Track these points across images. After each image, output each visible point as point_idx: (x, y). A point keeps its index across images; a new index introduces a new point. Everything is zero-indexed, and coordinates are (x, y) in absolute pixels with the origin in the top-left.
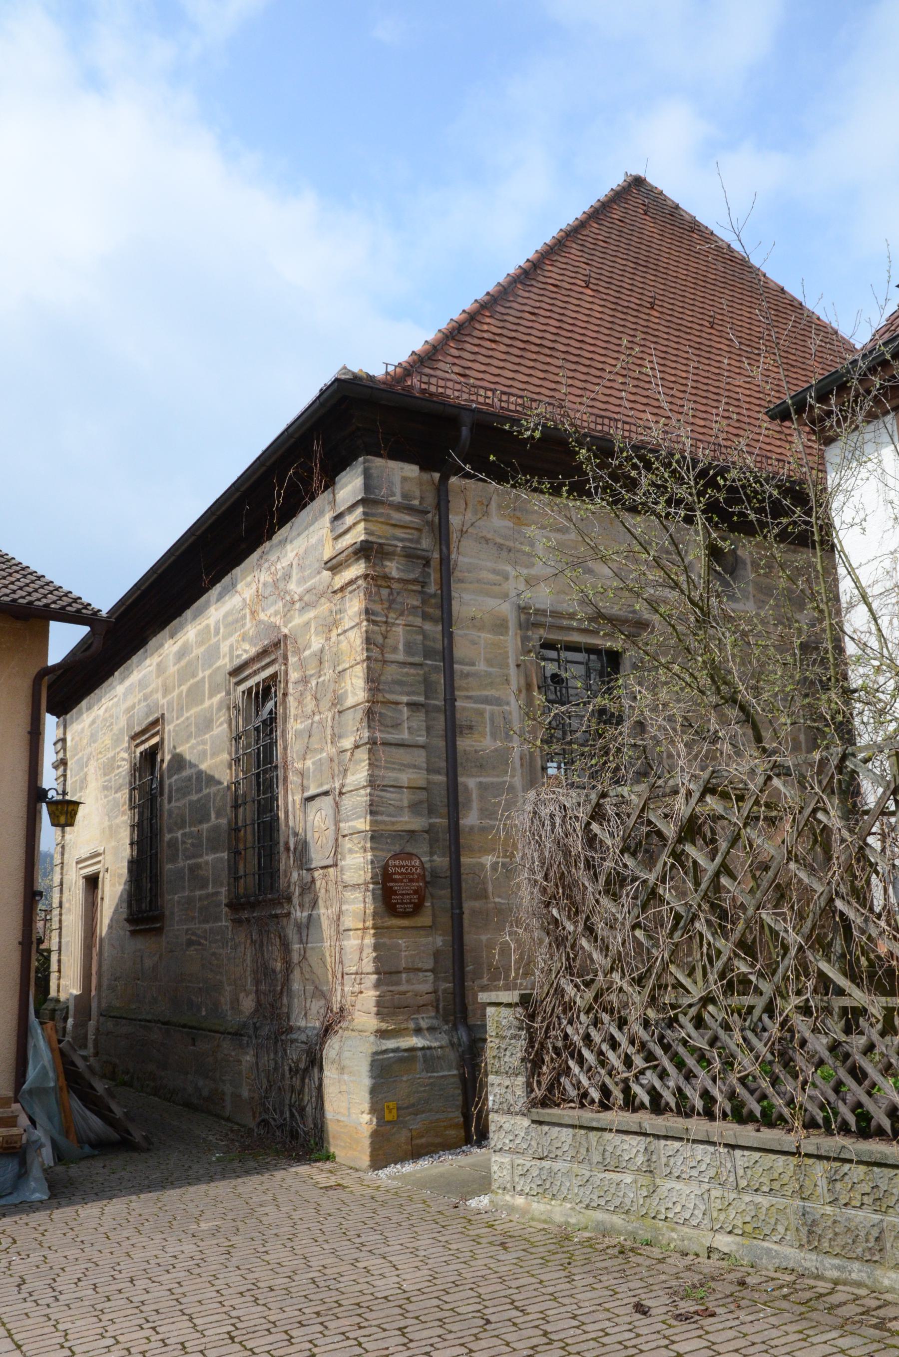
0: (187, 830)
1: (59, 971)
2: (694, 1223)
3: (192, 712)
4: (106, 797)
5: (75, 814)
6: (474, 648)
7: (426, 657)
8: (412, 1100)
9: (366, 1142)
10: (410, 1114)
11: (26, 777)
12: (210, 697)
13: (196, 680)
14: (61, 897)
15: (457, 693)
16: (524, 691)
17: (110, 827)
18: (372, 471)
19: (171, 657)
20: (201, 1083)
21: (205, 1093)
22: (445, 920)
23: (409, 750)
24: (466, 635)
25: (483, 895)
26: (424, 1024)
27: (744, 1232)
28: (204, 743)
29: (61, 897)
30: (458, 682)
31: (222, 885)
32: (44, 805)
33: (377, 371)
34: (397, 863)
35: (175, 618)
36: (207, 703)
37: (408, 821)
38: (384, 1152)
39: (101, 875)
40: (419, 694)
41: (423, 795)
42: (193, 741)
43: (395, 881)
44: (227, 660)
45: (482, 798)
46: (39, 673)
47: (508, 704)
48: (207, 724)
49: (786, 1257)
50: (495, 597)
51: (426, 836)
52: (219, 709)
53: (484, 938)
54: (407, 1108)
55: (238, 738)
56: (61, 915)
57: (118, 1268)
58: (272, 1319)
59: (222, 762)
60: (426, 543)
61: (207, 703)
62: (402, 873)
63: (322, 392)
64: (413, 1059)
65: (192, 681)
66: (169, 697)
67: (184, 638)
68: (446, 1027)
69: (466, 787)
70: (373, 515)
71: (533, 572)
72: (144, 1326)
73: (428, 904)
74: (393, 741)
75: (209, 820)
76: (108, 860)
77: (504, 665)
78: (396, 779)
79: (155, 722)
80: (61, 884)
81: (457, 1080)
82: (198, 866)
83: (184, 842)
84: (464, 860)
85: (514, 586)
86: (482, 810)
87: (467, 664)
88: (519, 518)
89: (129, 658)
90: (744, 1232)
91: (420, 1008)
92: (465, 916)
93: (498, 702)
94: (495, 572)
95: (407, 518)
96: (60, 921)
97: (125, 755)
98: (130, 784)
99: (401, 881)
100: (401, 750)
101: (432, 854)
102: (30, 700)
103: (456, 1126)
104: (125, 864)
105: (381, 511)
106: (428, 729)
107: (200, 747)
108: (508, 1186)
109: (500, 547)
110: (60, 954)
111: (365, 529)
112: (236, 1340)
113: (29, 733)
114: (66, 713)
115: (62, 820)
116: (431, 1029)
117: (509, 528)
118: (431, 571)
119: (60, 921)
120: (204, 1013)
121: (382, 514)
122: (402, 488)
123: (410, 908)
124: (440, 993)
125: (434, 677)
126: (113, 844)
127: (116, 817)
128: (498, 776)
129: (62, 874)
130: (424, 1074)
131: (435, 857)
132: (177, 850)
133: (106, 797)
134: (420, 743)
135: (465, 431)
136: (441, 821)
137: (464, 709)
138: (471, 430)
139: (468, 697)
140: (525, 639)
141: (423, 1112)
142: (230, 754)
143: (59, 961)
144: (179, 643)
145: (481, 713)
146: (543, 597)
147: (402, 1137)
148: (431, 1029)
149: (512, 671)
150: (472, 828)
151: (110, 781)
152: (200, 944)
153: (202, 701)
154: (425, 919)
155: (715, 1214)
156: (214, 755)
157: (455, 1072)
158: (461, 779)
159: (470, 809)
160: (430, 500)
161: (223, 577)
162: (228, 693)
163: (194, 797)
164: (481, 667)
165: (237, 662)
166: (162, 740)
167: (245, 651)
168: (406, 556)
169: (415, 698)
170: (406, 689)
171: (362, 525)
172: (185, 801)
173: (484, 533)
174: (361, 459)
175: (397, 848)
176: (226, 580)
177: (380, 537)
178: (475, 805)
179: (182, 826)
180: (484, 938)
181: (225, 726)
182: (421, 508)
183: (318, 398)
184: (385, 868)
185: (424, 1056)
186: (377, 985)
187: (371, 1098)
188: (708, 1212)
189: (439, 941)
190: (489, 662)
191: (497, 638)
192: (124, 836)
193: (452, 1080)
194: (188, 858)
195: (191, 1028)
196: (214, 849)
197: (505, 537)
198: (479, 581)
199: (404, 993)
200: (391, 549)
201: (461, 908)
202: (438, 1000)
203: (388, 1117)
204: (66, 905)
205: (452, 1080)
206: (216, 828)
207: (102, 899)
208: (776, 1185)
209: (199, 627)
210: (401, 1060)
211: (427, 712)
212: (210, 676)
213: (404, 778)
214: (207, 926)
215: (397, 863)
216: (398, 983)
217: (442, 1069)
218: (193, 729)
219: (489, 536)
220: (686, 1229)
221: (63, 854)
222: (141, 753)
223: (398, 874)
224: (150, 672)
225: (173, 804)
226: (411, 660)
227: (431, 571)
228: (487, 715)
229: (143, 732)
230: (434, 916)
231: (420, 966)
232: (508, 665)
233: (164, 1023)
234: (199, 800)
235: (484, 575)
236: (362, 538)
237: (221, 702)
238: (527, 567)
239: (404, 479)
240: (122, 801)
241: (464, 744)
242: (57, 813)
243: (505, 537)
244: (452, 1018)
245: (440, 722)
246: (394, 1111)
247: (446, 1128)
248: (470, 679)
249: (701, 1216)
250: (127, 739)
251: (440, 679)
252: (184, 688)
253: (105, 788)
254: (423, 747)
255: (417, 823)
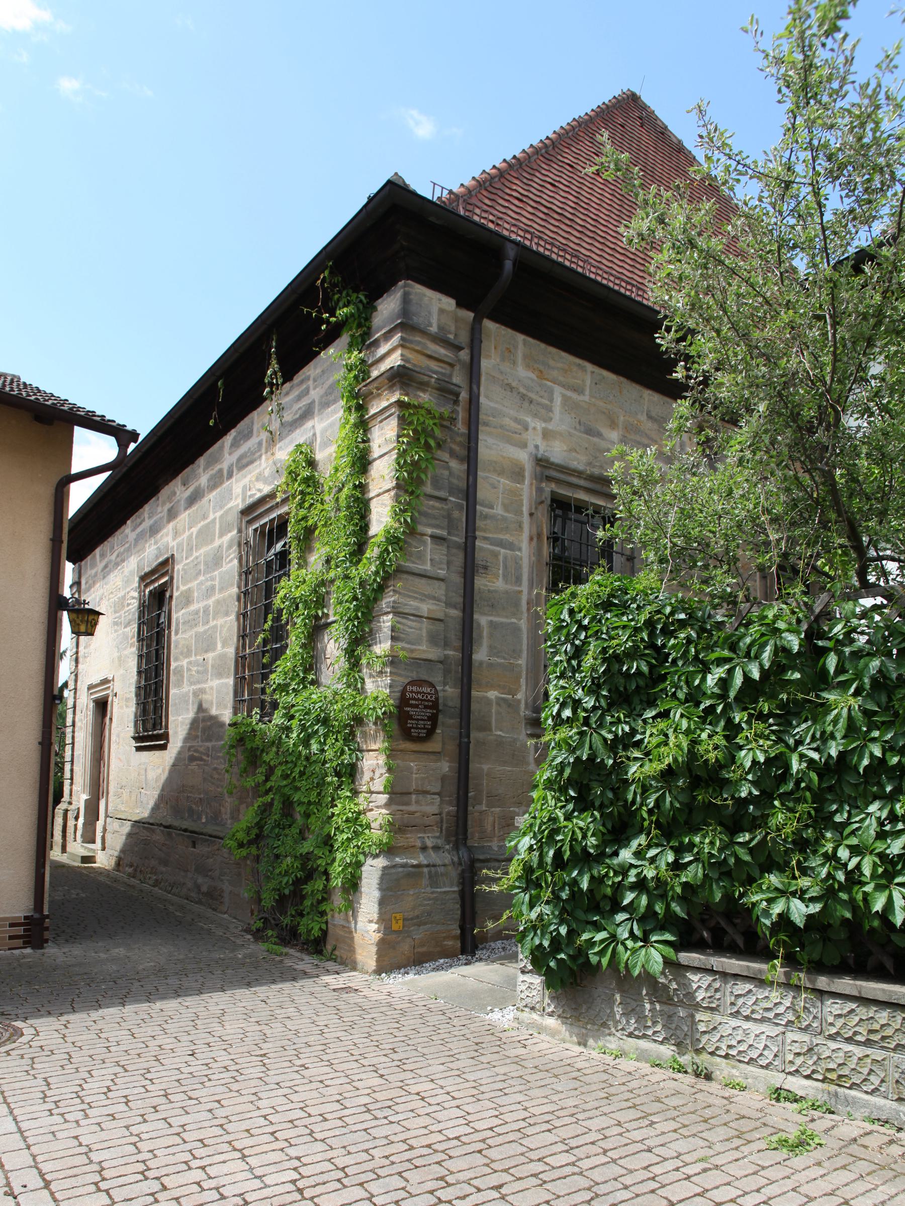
0: (193, 658)
1: (72, 779)
2: (764, 1062)
3: (202, 551)
4: (116, 631)
5: (96, 624)
6: (493, 490)
7: (451, 494)
8: (417, 913)
9: (374, 949)
10: (414, 925)
11: (48, 584)
12: (221, 535)
13: (207, 521)
14: (74, 718)
15: (477, 533)
16: (535, 539)
17: (120, 658)
18: (412, 297)
19: (182, 502)
20: (200, 880)
21: (204, 889)
22: (452, 747)
23: (430, 581)
24: (487, 477)
25: (486, 727)
26: (429, 843)
27: (727, 1054)
28: (213, 579)
29: (74, 718)
30: (479, 523)
31: (226, 707)
32: (65, 613)
33: (425, 191)
34: (414, 689)
35: (187, 466)
36: (217, 543)
37: (426, 650)
38: (392, 960)
39: (110, 699)
40: (442, 528)
41: (440, 626)
42: (202, 578)
43: (412, 706)
44: (239, 501)
45: (491, 636)
46: (61, 480)
47: (520, 549)
48: (216, 560)
49: (880, 1108)
50: (515, 445)
51: (441, 666)
52: (230, 547)
53: (485, 767)
54: (412, 919)
55: (247, 573)
56: (73, 732)
57: (148, 1076)
58: (340, 1163)
59: (230, 596)
60: (458, 378)
61: (217, 543)
62: (418, 699)
63: (371, 200)
64: (420, 875)
65: (202, 523)
66: (179, 539)
67: (196, 484)
68: (447, 847)
69: (479, 625)
70: (411, 342)
71: (550, 426)
72: (205, 1185)
73: (438, 731)
74: (416, 571)
75: (214, 649)
76: (117, 686)
77: (519, 513)
78: (417, 609)
79: (165, 563)
80: (74, 707)
81: (457, 896)
82: (203, 691)
83: (189, 670)
84: (474, 693)
85: (534, 439)
86: (491, 647)
87: (486, 506)
88: (541, 371)
89: (141, 507)
90: (727, 1054)
91: (426, 827)
92: (471, 746)
93: (511, 546)
94: (516, 420)
95: (442, 351)
96: (73, 737)
97: (136, 594)
98: (139, 619)
99: (416, 706)
100: (424, 581)
101: (445, 684)
102: (52, 508)
103: (454, 938)
104: (133, 689)
105: (418, 339)
106: (449, 563)
107: (209, 583)
108: (537, 1006)
109: (523, 397)
110: (72, 764)
111: (402, 355)
112: (308, 1193)
113: (51, 540)
114: (81, 560)
115: (83, 628)
116: (436, 848)
117: (532, 380)
118: (460, 409)
119: (73, 737)
120: (204, 820)
121: (419, 343)
122: (439, 320)
123: (423, 733)
124: (444, 815)
125: (456, 514)
126: (122, 671)
127: (125, 649)
128: (507, 617)
129: (75, 698)
130: (429, 889)
131: (447, 688)
132: (183, 677)
133: (116, 631)
134: (441, 576)
135: (508, 265)
136: (453, 654)
137: (481, 549)
138: (514, 265)
139: (485, 538)
140: (540, 490)
141: (425, 924)
142: (239, 587)
143: (72, 770)
144: (191, 489)
145: (496, 555)
146: (557, 452)
147: (405, 947)
148: (436, 848)
149: (526, 519)
150: (481, 663)
151: (120, 617)
152: (202, 760)
153: (213, 540)
154: (434, 745)
155: (790, 1057)
156: (222, 589)
157: (456, 889)
158: (476, 616)
159: (480, 645)
160: (464, 338)
161: (239, 421)
162: (240, 531)
163: (201, 629)
164: (499, 510)
165: (249, 501)
166: (172, 578)
167: (259, 490)
168: (438, 389)
169: (438, 532)
170: (433, 522)
171: (399, 352)
172: (192, 632)
173: (510, 381)
174: (401, 283)
175: (414, 675)
176: (242, 425)
177: (415, 365)
178: (485, 642)
179: (188, 654)
180: (485, 767)
181: (236, 562)
182: (456, 343)
183: (365, 206)
184: (403, 692)
185: (430, 872)
186: (387, 805)
187: (380, 909)
188: (780, 1054)
189: (445, 767)
190: (506, 508)
191: (514, 485)
192: (132, 665)
193: (453, 896)
194: (192, 684)
195: (192, 832)
196: (220, 675)
197: (528, 388)
198: (502, 427)
199: (413, 813)
200: (426, 379)
201: (468, 736)
202: (442, 821)
203: (395, 927)
204: (78, 724)
205: (453, 896)
206: (222, 657)
207: (111, 719)
208: (876, 1037)
209: (211, 472)
210: (409, 875)
211: (448, 547)
212: (221, 517)
213: (425, 608)
214: (209, 744)
215: (414, 689)
216: (408, 804)
217: (445, 886)
218: (202, 567)
219: (514, 384)
220: (750, 1068)
221: (76, 681)
222: (150, 592)
223: (415, 699)
224: (161, 518)
225: (179, 636)
226: (437, 493)
227: (460, 409)
228: (501, 558)
229: (153, 572)
230: (444, 744)
231: (428, 788)
232: (521, 513)
233: (166, 827)
234: (205, 632)
235: (507, 421)
236: (399, 363)
237: (231, 540)
238: (545, 421)
239: (441, 311)
240: (130, 635)
241: (481, 582)
242: (78, 621)
243: (528, 388)
244: (453, 839)
245: (459, 559)
246: (401, 922)
247: (445, 938)
248: (488, 521)
249: (771, 1057)
250: (137, 579)
251: (460, 516)
252: (194, 530)
253: (116, 624)
254: (442, 580)
255: (433, 653)
